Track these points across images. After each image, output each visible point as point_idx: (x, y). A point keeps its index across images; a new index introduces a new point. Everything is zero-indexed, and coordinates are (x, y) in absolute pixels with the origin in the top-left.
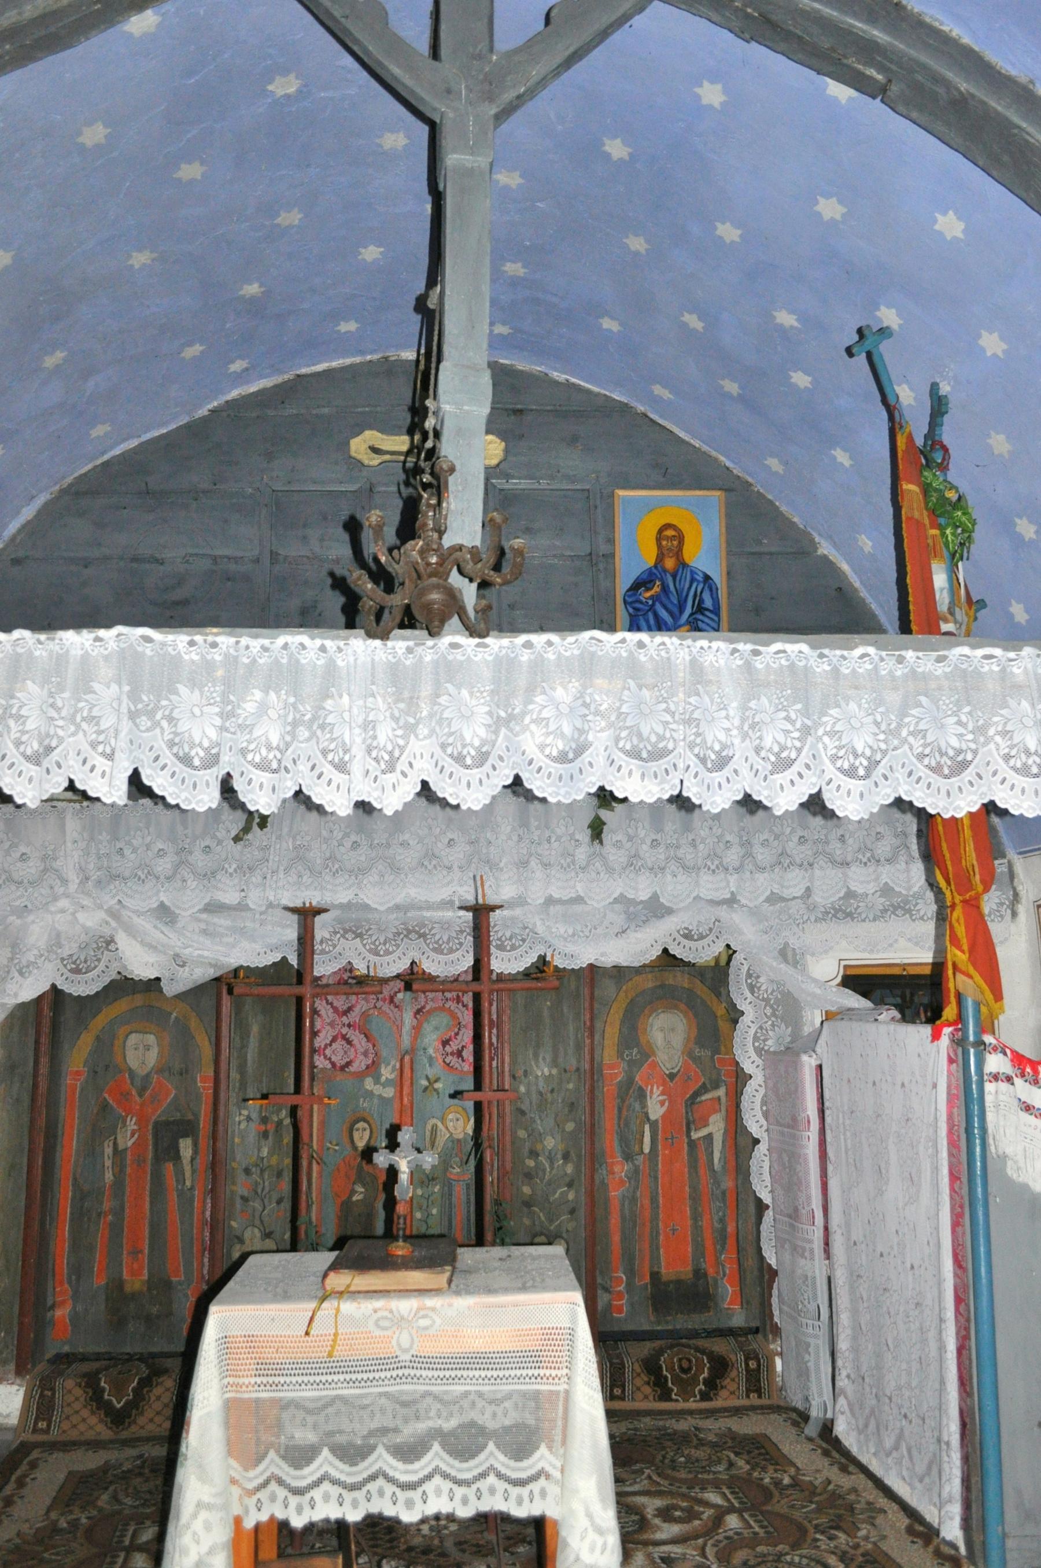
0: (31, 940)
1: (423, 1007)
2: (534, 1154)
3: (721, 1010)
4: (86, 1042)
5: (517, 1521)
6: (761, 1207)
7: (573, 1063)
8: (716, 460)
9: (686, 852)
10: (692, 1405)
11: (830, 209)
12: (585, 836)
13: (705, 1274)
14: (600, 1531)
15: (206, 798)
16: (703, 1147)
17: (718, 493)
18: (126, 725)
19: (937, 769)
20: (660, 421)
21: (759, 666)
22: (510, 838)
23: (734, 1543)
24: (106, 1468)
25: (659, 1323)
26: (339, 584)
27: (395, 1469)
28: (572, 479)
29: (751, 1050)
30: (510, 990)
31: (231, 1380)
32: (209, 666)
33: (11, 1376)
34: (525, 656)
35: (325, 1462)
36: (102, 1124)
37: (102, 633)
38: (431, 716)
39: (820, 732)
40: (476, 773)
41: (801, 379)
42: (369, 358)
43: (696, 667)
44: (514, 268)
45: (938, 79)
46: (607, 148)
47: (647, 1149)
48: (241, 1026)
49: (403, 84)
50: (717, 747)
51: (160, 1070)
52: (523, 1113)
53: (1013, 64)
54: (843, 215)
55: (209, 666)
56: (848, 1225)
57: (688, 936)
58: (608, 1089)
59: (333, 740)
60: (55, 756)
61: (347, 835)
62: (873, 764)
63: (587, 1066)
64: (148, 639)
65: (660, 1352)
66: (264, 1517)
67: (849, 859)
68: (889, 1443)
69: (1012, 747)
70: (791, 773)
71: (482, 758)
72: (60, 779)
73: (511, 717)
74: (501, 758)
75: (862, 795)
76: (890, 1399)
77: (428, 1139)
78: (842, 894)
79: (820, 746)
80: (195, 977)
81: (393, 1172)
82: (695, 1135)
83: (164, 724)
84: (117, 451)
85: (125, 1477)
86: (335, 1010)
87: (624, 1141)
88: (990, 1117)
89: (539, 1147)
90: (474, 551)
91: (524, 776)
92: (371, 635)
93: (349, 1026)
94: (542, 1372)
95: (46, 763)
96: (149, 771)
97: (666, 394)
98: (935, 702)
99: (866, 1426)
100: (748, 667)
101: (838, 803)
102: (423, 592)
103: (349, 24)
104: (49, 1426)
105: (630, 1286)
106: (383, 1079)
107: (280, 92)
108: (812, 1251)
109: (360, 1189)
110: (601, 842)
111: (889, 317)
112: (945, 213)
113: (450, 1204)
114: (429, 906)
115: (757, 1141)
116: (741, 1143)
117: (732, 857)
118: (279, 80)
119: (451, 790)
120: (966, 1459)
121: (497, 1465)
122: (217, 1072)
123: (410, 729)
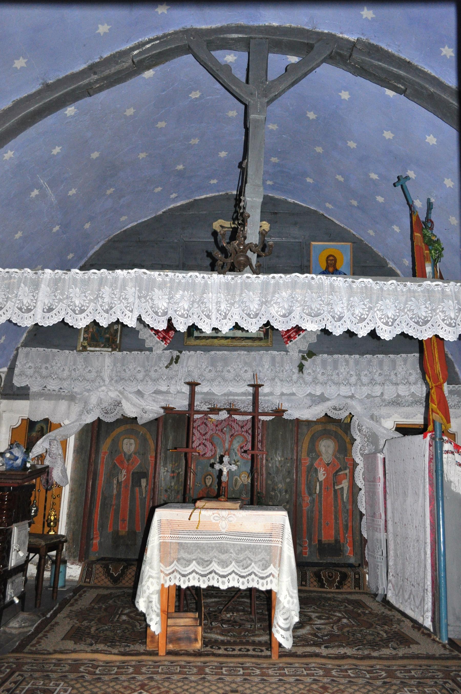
0: (92, 401)
2: (274, 490)
3: (348, 440)
4: (109, 441)
5: (262, 592)
6: (362, 515)
7: (290, 456)
8: (350, 231)
9: (335, 377)
10: (332, 590)
11: (388, 135)
12: (296, 370)
13: (340, 542)
14: (292, 597)
15: (162, 326)
16: (339, 492)
17: (350, 244)
18: (137, 301)
19: (417, 323)
20: (329, 217)
21: (354, 286)
22: (268, 370)
23: (344, 626)
24: (111, 594)
25: (321, 559)
26: (209, 255)
27: (219, 570)
28: (295, 238)
29: (359, 454)
31: (162, 535)
32: (164, 282)
33: (77, 562)
34: (272, 281)
35: (194, 566)
36: (113, 472)
37: (130, 271)
38: (239, 301)
39: (376, 309)
40: (254, 320)
41: (380, 199)
42: (221, 193)
43: (332, 286)
44: (274, 160)
45: (423, 87)
46: (308, 115)
47: (318, 492)
48: (166, 438)
49: (236, 92)
50: (339, 313)
51: (135, 453)
52: (270, 474)
53: (450, 82)
54: (393, 137)
55: (164, 282)
56: (393, 516)
57: (335, 409)
58: (303, 468)
59: (206, 307)
60: (113, 310)
61: (207, 367)
62: (394, 320)
63: (295, 458)
64: (145, 273)
65: (321, 570)
66: (172, 584)
67: (399, 382)
68: (406, 597)
69: (445, 316)
70: (364, 323)
71: (256, 315)
72: (115, 317)
73: (267, 301)
74: (263, 315)
75: (390, 332)
76: (407, 579)
78: (395, 396)
79: (376, 314)
80: (150, 417)
81: (221, 471)
82: (337, 488)
83: (150, 300)
84: (129, 226)
85: (118, 596)
86: (201, 434)
87: (309, 489)
88: (445, 467)
89: (276, 487)
90: (256, 246)
91: (271, 321)
92: (220, 273)
93: (206, 440)
94: (272, 539)
95: (110, 312)
96: (144, 316)
97: (330, 206)
98: (417, 300)
99: (399, 592)
100: (350, 286)
101: (382, 334)
102: (238, 258)
103: (219, 73)
104: (90, 581)
105: (310, 545)
107: (194, 97)
108: (380, 529)
110: (302, 372)
111: (411, 174)
112: (429, 136)
114: (237, 394)
115: (360, 489)
116: (354, 490)
117: (353, 380)
118: (193, 93)
119: (245, 325)
120: (433, 595)
121: (255, 571)
122: (156, 454)
123: (233, 304)
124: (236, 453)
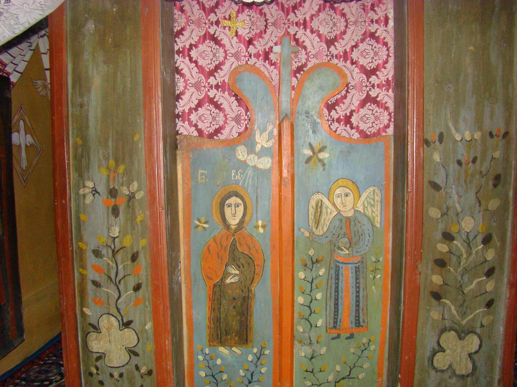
1: (305, 65)
77: (311, 217)
86: (201, 69)
93: (217, 87)
106: (258, 147)
109: (233, 271)
113: (337, 288)
124: (314, 125)
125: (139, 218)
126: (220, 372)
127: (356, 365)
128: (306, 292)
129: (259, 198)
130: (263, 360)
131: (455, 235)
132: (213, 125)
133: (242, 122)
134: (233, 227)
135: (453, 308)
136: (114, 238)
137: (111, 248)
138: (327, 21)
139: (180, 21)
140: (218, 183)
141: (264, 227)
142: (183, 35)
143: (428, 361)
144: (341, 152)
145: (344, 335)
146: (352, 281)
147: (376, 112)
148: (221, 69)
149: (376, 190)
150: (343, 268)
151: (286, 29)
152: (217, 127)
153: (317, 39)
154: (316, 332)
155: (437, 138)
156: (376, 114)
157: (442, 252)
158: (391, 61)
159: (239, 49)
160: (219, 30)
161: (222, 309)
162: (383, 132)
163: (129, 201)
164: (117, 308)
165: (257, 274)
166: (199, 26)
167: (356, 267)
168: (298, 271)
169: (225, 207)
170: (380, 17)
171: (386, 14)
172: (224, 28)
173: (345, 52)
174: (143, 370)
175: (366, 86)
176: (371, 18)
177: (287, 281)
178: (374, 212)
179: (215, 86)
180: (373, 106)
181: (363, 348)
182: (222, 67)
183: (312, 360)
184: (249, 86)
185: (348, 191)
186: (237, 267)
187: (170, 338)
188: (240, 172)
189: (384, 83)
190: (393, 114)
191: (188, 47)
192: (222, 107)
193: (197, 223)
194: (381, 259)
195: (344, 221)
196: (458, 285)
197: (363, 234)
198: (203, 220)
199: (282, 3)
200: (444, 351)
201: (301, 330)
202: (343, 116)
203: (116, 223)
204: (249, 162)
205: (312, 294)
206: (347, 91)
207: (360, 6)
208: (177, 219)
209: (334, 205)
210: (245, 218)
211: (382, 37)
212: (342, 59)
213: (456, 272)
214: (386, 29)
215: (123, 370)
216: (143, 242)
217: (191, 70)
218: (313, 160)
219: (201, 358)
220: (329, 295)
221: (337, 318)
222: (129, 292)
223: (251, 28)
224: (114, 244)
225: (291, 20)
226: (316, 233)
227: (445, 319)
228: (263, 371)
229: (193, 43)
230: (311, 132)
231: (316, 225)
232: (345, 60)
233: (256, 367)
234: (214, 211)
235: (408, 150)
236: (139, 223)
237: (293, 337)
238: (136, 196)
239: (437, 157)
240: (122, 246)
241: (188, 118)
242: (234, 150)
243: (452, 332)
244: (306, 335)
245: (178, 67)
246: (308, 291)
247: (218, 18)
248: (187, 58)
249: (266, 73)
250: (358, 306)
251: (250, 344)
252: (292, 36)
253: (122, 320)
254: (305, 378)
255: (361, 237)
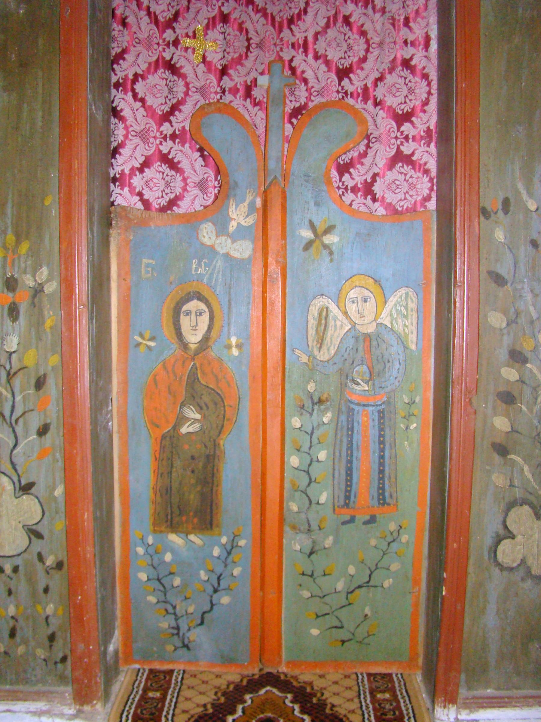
30: (110, 713)
77: (312, 332)
86: (150, 111)
93: (173, 137)
109: (192, 413)
113: (350, 443)
125: (49, 323)
126: (171, 573)
127: (379, 566)
128: (302, 449)
129: (232, 303)
130: (235, 556)
131: (529, 355)
132: (167, 194)
133: (210, 190)
134: (193, 347)
135: (526, 468)
136: (11, 354)
137: (5, 368)
138: (338, 41)
139: (121, 38)
140: (172, 278)
141: (239, 346)
142: (124, 59)
143: (489, 553)
144: (358, 234)
145: (361, 518)
146: (373, 433)
147: (411, 177)
148: (180, 111)
149: (410, 293)
150: (360, 413)
151: (278, 52)
152: (172, 196)
153: (323, 68)
154: (318, 512)
155: (500, 207)
156: (411, 180)
157: (508, 381)
158: (434, 100)
159: (208, 82)
160: (178, 53)
161: (174, 474)
162: (421, 207)
163: (34, 296)
164: (12, 463)
165: (228, 420)
166: (149, 47)
167: (379, 411)
168: (291, 416)
169: (182, 315)
170: (418, 36)
171: (427, 33)
172: (186, 49)
173: (366, 89)
174: (50, 561)
175: (396, 138)
176: (405, 37)
177: (274, 432)
178: (407, 327)
179: (171, 135)
180: (407, 169)
181: (389, 539)
182: (181, 107)
183: (313, 557)
184: (220, 133)
185: (367, 293)
186: (198, 408)
187: (91, 509)
188: (205, 263)
189: (422, 134)
190: (435, 180)
191: (131, 77)
192: (179, 166)
193: (139, 340)
194: (417, 399)
195: (361, 339)
196: (535, 434)
197: (391, 360)
198: (147, 335)
199: (272, 14)
200: (513, 537)
201: (295, 508)
202: (361, 183)
203: (14, 330)
204: (218, 249)
205: (311, 452)
206: (368, 146)
207: (389, 19)
208: (108, 322)
209: (346, 313)
210: (210, 333)
211: (420, 67)
212: (360, 99)
213: (531, 412)
214: (426, 54)
215: (19, 561)
216: (54, 360)
217: (135, 111)
218: (315, 245)
219: (140, 550)
220: (337, 454)
221: (350, 491)
222: (31, 438)
223: (225, 50)
224: (10, 362)
225: (285, 39)
226: (318, 357)
227: (513, 486)
228: (236, 572)
229: (140, 72)
230: (312, 203)
231: (318, 346)
232: (365, 100)
233: (226, 566)
234: (165, 322)
235: (456, 223)
236: (48, 330)
237: (282, 520)
238: (45, 288)
239: (500, 235)
240: (22, 367)
241: (130, 183)
242: (196, 230)
243: (526, 507)
244: (303, 516)
245: (116, 106)
246: (305, 448)
247: (178, 36)
248: (130, 94)
249: (248, 118)
250: (381, 472)
251: (216, 530)
252: (287, 63)
253: (19, 481)
254: (300, 585)
255: (387, 365)
